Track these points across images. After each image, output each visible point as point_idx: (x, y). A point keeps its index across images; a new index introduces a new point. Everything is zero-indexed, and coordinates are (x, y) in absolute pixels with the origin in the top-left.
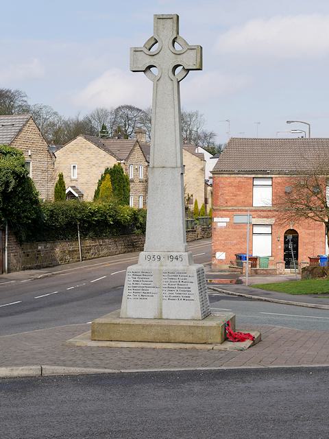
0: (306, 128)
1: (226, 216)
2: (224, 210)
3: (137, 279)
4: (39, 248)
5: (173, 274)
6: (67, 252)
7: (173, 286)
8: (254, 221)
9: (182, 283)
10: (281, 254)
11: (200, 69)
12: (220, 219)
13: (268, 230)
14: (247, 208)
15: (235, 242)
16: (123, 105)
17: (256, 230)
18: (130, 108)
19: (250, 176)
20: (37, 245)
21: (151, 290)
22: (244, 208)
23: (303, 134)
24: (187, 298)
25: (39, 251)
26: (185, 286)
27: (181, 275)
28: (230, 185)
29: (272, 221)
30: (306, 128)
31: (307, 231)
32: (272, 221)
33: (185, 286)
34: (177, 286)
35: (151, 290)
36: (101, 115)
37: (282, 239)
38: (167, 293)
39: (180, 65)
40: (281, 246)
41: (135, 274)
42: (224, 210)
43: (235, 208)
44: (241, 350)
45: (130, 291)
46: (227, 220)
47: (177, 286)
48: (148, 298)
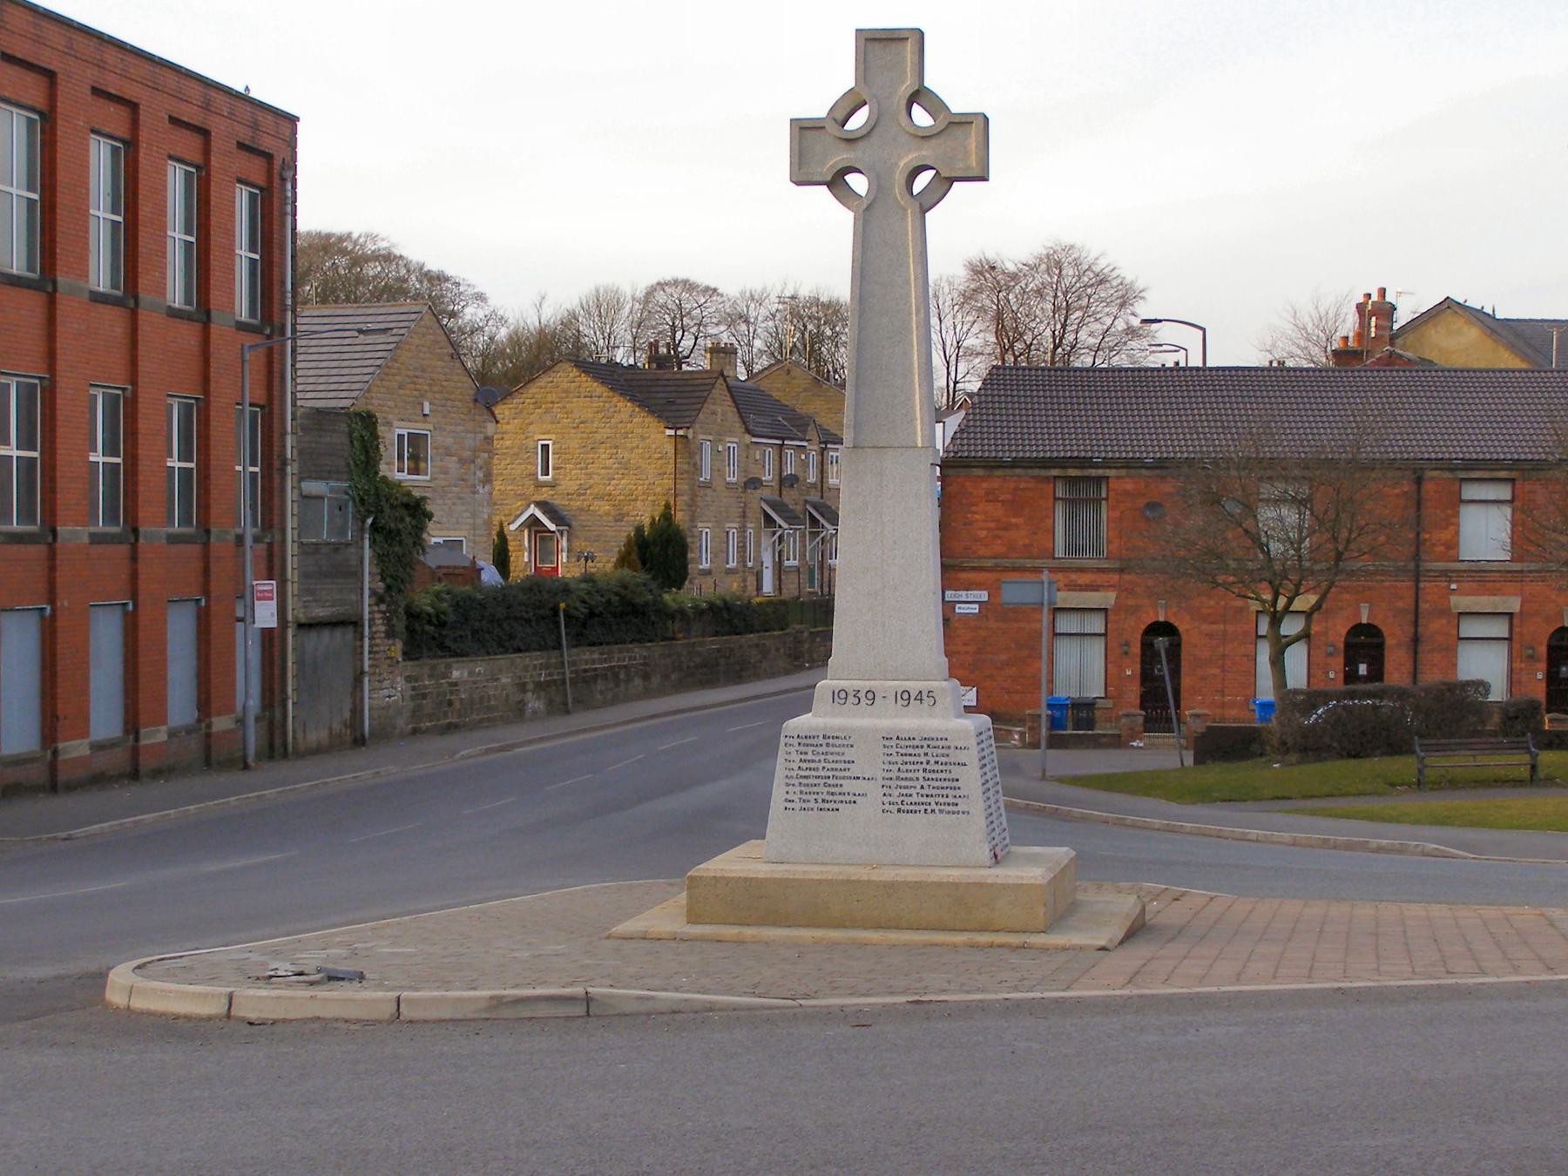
0: (1192, 339)
1: (979, 586)
2: (974, 569)
3: (810, 757)
4: (456, 674)
5: (905, 747)
6: (531, 686)
7: (909, 775)
8: (1065, 598)
9: (936, 767)
10: (1133, 692)
11: (984, 178)
12: (963, 595)
13: (1096, 624)
14: (1038, 563)
15: (1004, 657)
16: (668, 278)
17: (1066, 624)
18: (688, 286)
19: (1043, 473)
20: (449, 667)
21: (848, 786)
22: (1029, 563)
23: (1180, 357)
24: (952, 808)
25: (456, 684)
26: (943, 776)
27: (932, 743)
28: (991, 497)
29: (1107, 598)
30: (1192, 339)
31: (1205, 627)
32: (1107, 598)
33: (943, 776)
34: (921, 775)
35: (848, 786)
36: (604, 306)
37: (1136, 649)
38: (896, 792)
39: (933, 168)
40: (1131, 670)
41: (806, 740)
42: (974, 569)
43: (1007, 563)
44: (944, 991)
45: (791, 789)
46: (983, 596)
47: (921, 775)
48: (839, 806)
